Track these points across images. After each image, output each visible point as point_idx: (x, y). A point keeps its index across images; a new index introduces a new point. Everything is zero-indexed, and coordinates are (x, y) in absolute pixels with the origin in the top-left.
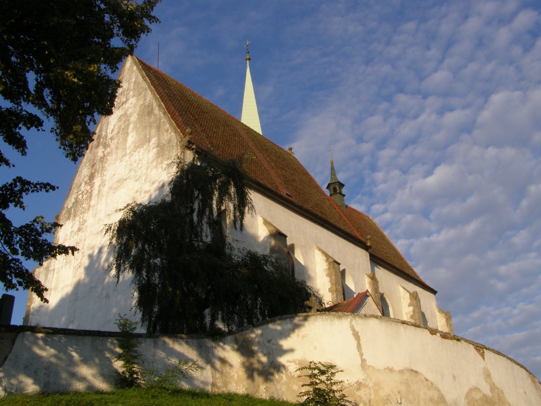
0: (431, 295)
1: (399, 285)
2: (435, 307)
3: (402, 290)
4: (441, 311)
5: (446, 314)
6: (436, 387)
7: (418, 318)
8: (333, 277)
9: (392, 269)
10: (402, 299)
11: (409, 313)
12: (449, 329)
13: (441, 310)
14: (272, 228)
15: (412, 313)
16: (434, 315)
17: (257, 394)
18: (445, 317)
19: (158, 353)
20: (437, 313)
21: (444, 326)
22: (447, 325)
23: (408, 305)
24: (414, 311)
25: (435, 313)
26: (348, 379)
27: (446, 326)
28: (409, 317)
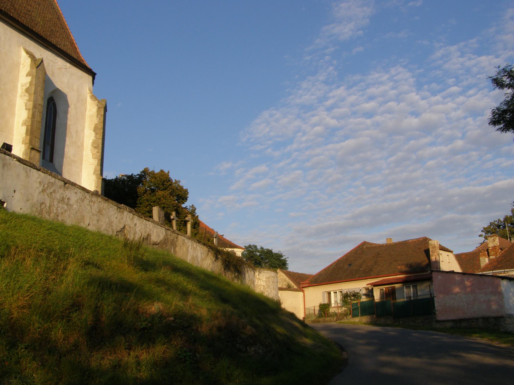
1: (22, 47)
3: (23, 54)
4: (94, 97)
5: (99, 102)
7: (33, 93)
8: (404, 242)
9: (12, 23)
10: (21, 66)
11: (26, 84)
12: (98, 120)
13: (94, 96)
14: (439, 259)
15: (28, 85)
17: (82, 223)
18: (97, 105)
20: (89, 100)
21: (93, 116)
22: (98, 115)
23: (26, 74)
24: (31, 83)
25: (86, 98)
26: (447, 255)
27: (96, 116)
28: (24, 90)
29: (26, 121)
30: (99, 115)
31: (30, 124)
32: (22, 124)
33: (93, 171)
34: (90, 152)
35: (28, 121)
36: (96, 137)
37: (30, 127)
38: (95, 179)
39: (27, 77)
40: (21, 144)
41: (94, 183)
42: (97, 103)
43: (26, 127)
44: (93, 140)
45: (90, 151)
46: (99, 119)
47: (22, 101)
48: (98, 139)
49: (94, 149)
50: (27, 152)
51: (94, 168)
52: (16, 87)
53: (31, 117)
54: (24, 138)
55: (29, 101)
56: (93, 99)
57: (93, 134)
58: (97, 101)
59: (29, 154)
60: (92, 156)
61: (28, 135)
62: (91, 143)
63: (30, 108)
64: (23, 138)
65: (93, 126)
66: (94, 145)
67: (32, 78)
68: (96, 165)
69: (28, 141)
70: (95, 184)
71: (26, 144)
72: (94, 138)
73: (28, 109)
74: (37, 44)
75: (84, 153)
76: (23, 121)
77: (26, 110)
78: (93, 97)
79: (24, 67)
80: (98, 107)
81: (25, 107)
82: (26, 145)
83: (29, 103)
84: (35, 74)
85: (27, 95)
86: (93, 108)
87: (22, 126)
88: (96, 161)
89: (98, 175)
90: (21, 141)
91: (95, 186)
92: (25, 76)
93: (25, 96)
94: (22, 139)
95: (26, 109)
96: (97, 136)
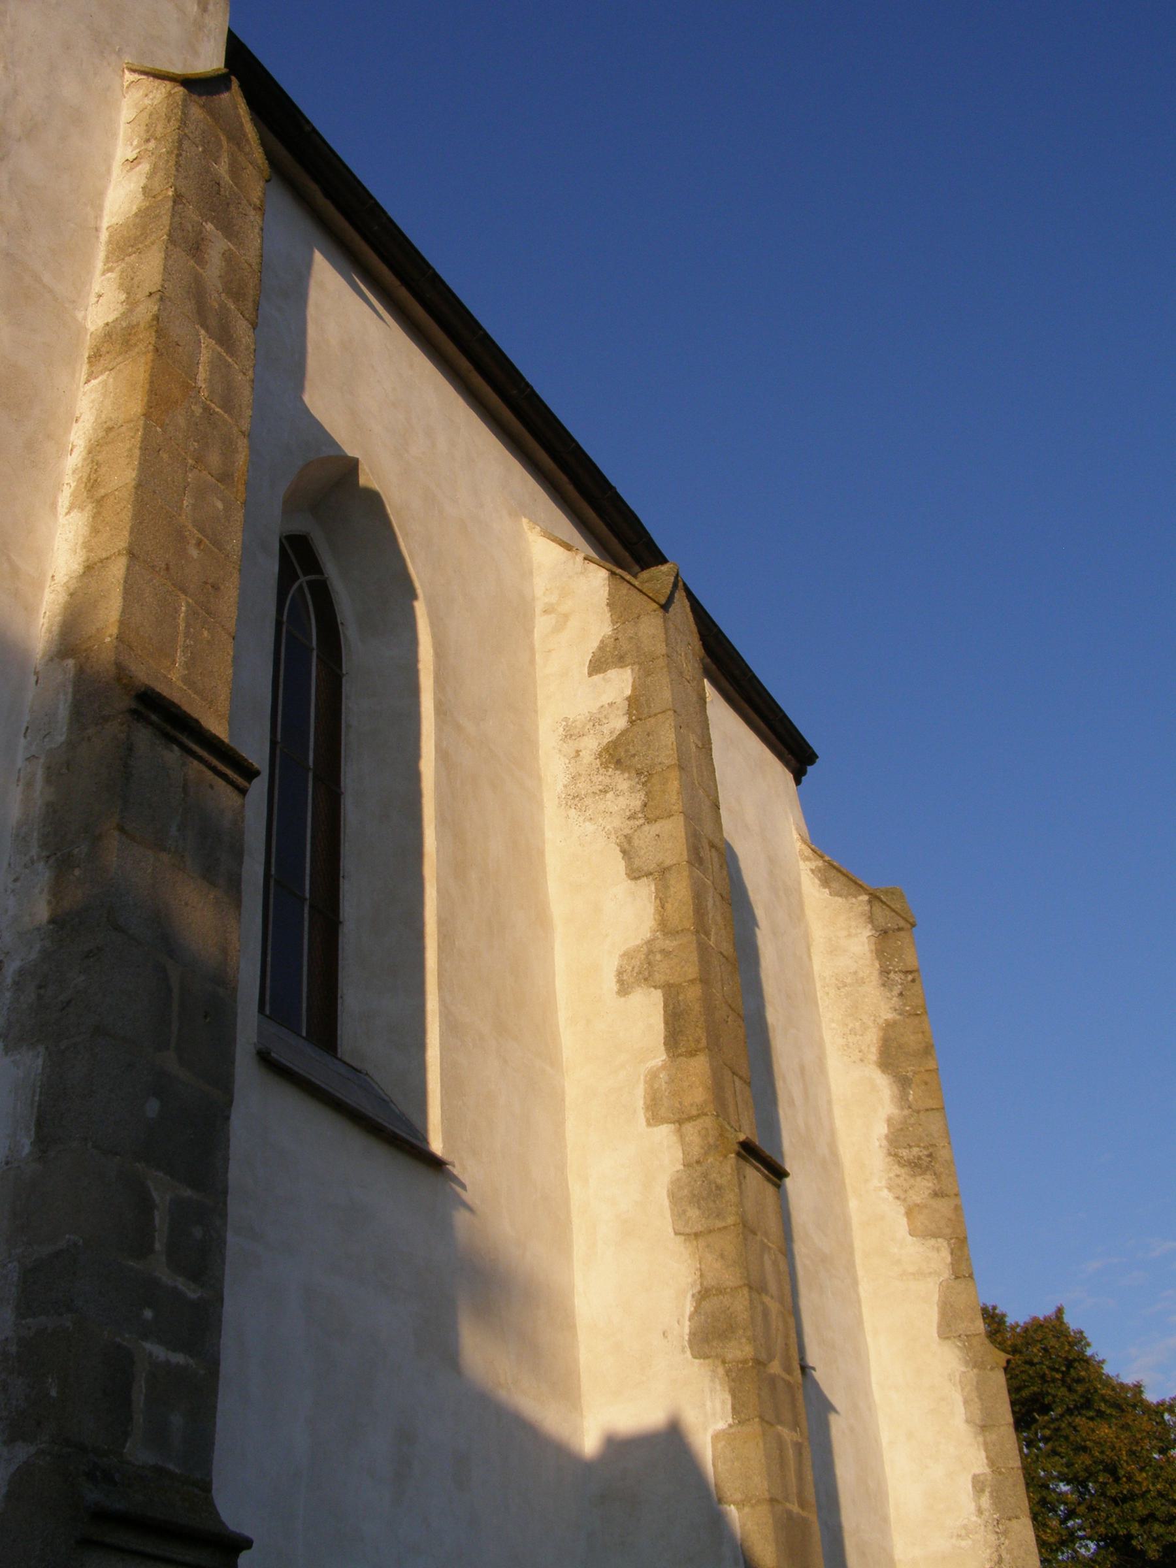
0: (777, 773)
2: (799, 845)
5: (874, 898)
6: (970, 1265)
7: (673, 761)
10: (542, 624)
11: (596, 721)
15: (619, 723)
16: (792, 894)
18: (871, 919)
19: (1158, 1551)
21: (861, 982)
22: (885, 972)
24: (637, 706)
28: (587, 757)
29: (650, 952)
30: (892, 975)
31: (692, 971)
32: (621, 982)
33: (934, 1316)
34: (885, 1193)
35: (666, 953)
36: (902, 1099)
37: (693, 994)
38: (963, 1369)
39: (597, 678)
40: (642, 1120)
41: (958, 1398)
42: (867, 908)
43: (657, 996)
44: (889, 1121)
45: (890, 1189)
46: (901, 994)
47: (590, 827)
48: (918, 1112)
49: (914, 1176)
50: (705, 1175)
51: (936, 1298)
52: (527, 740)
53: (689, 924)
54: (663, 1075)
55: (649, 821)
56: (834, 885)
57: (884, 1085)
58: (865, 898)
59: (731, 1196)
60: (904, 1220)
61: (692, 1054)
62: (884, 1143)
63: (668, 862)
64: (653, 1076)
65: (872, 1038)
66: (904, 1153)
67: (645, 672)
68: (946, 1274)
69: (698, 1095)
70: (966, 1402)
71: (690, 1118)
72: (896, 1111)
73: (648, 874)
74: (576, 526)
75: (853, 1204)
76: (627, 955)
77: (636, 878)
78: (833, 873)
79: (559, 627)
80: (875, 928)
81: (621, 865)
82: (690, 1128)
83: (652, 830)
84: (661, 648)
85: (622, 782)
86: (849, 936)
87: (624, 989)
88: (938, 1250)
89: (975, 1341)
90: (640, 1103)
91: (967, 1421)
92: (586, 671)
93: (610, 795)
94: (640, 1091)
95: (635, 874)
96: (911, 1098)
